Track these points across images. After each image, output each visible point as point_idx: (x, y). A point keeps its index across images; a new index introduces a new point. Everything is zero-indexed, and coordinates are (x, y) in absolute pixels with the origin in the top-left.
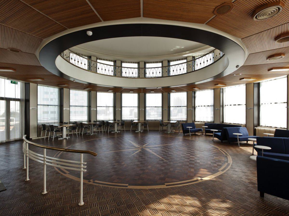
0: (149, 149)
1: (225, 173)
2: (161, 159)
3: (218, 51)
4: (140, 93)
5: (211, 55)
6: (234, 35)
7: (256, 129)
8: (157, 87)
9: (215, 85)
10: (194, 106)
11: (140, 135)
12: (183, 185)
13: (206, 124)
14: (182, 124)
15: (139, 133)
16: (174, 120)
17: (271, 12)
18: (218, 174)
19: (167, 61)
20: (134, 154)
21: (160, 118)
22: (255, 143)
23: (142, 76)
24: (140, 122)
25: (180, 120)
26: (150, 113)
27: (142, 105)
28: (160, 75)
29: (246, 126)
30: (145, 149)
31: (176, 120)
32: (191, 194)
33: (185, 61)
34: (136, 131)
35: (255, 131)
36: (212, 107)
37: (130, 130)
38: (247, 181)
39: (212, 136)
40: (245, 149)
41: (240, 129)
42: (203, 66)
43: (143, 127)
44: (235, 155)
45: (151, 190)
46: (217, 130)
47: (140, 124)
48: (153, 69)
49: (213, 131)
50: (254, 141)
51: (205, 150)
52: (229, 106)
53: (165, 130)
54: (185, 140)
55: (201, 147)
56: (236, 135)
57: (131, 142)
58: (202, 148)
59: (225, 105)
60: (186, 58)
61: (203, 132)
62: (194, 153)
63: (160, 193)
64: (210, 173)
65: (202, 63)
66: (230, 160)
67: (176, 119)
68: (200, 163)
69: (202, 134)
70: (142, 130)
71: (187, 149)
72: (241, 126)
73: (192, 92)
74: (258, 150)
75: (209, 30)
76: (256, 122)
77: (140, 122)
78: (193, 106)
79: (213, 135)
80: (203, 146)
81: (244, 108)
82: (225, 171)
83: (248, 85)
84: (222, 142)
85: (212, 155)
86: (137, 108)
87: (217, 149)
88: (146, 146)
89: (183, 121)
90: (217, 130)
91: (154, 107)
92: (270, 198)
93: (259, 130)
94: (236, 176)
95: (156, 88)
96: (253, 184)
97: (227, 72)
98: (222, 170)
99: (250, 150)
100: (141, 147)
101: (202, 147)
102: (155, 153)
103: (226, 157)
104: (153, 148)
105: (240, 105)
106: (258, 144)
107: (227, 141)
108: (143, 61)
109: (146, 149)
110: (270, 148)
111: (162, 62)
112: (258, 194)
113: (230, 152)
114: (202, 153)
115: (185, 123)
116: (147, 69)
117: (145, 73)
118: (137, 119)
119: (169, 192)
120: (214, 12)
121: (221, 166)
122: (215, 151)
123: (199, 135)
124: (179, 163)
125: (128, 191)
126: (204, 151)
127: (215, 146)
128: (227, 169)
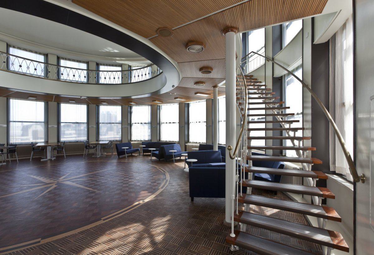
0: (71, 181)
1: (164, 189)
2: (91, 190)
3: (155, 67)
4: (49, 102)
5: (148, 70)
6: (172, 58)
7: (186, 145)
8: (81, 97)
9: (153, 101)
10: (130, 123)
11: (49, 165)
12: (124, 213)
13: (144, 143)
14: (116, 145)
15: (49, 162)
16: (106, 141)
17: (198, 49)
18: (158, 193)
19: (95, 64)
20: (45, 193)
21: (84, 138)
22: (187, 158)
23: (53, 75)
24: (50, 146)
25: (113, 139)
26: (64, 131)
27: (53, 119)
28: (120, 82)
29: (179, 143)
30: (62, 182)
31: (108, 140)
32: (134, 221)
33: (120, 69)
34: (42, 160)
35: (186, 146)
36: (150, 124)
37: (30, 159)
38: (182, 192)
39: (149, 155)
40: (178, 165)
41: (175, 146)
42: (141, 79)
43: (56, 152)
44: (171, 171)
45: (82, 233)
46: (155, 149)
47: (49, 149)
48: (114, 73)
49: (151, 150)
50: (186, 156)
51: (145, 171)
52: (165, 124)
53: (93, 154)
54: (119, 163)
55: (139, 168)
56: (172, 152)
57: (35, 177)
58: (141, 169)
59: (162, 123)
60: (121, 65)
61: (140, 152)
62: (133, 176)
63: (96, 231)
64: (150, 194)
65: (140, 76)
66: (168, 176)
67: (108, 138)
68: (141, 185)
69: (140, 155)
70: (54, 157)
71: (125, 173)
72: (175, 143)
73: (127, 106)
74: (189, 163)
75: (116, 27)
76: (186, 139)
77: (50, 146)
78: (129, 122)
79: (151, 155)
80: (142, 167)
81: (177, 126)
82: (164, 188)
83: (180, 104)
84: (160, 160)
85: (151, 174)
86: (43, 123)
87: (156, 168)
88: (64, 178)
89: (117, 141)
90: (155, 149)
91: (71, 124)
92: (197, 200)
93: (188, 145)
94: (173, 190)
95: (79, 97)
96: (186, 193)
97: (163, 91)
98: (162, 188)
99: (182, 165)
100: (56, 182)
101: (141, 168)
102: (81, 185)
103: (164, 174)
104: (77, 180)
105: (174, 123)
106: (189, 158)
107: (164, 159)
108: (95, 62)
109: (64, 182)
110: (196, 160)
111: (87, 63)
112: (190, 199)
113: (167, 169)
114: (142, 174)
115: (119, 143)
116: (101, 73)
117: (98, 77)
118: (43, 140)
119: (109, 226)
120: (157, 31)
121: (160, 184)
122: (154, 170)
123: (136, 155)
124: (117, 190)
125: (43, 247)
126: (144, 172)
127: (153, 166)
128: (166, 186)
